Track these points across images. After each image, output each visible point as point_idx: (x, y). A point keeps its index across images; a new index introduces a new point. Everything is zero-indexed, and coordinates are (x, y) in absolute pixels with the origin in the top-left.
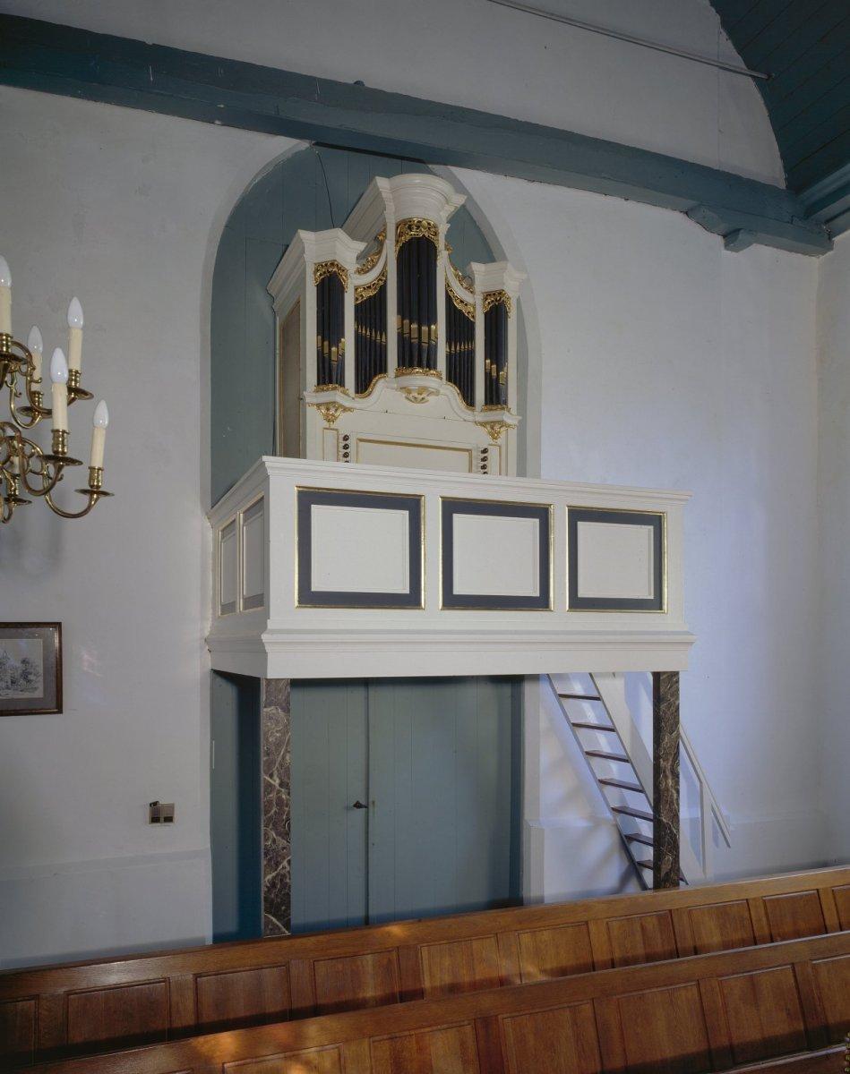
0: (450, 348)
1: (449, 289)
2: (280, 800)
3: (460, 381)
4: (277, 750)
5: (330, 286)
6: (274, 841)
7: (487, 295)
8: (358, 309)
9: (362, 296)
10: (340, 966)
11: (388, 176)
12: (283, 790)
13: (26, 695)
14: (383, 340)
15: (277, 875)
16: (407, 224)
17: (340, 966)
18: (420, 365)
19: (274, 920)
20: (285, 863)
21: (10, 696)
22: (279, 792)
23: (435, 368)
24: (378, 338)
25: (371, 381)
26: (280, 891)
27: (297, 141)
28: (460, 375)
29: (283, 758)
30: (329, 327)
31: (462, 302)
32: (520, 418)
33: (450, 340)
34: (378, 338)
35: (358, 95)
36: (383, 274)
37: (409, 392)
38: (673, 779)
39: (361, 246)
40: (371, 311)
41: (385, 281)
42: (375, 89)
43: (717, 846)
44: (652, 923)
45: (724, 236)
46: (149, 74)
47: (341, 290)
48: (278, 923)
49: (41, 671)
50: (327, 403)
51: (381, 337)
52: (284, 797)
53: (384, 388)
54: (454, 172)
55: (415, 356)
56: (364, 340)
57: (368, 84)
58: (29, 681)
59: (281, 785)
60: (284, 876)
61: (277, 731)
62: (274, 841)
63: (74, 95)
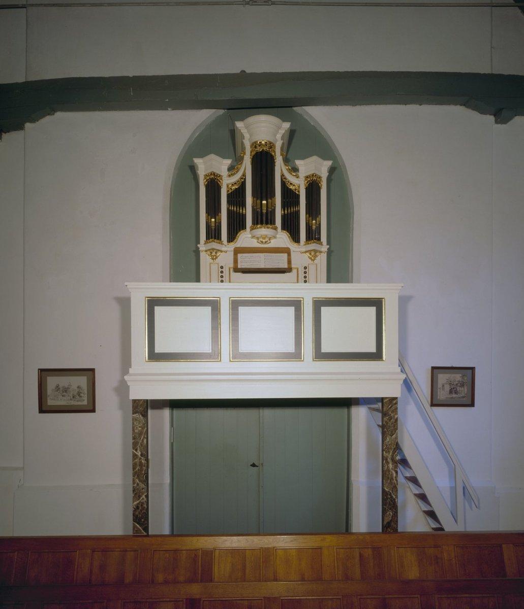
0: (284, 211)
1: (283, 177)
2: (141, 463)
3: (291, 229)
4: (139, 437)
5: (213, 185)
6: (138, 484)
7: (307, 177)
8: (229, 196)
9: (231, 189)
10: (167, 555)
11: (242, 119)
12: (143, 458)
13: (80, 403)
14: (244, 211)
15: (140, 502)
16: (254, 145)
17: (167, 555)
18: (262, 223)
19: (138, 526)
20: (144, 496)
21: (72, 404)
22: (140, 459)
23: (274, 224)
24: (241, 211)
25: (237, 234)
26: (141, 511)
27: (214, 110)
28: (291, 226)
29: (143, 441)
30: (213, 208)
31: (291, 184)
32: (328, 246)
33: (284, 206)
34: (241, 211)
35: (244, 78)
36: (244, 175)
37: (258, 238)
38: (392, 464)
39: (228, 162)
40: (237, 197)
41: (245, 179)
42: (145, 76)
43: (472, 509)
44: (368, 553)
45: (495, 115)
46: (130, 91)
47: (219, 188)
48: (140, 528)
49: (86, 392)
50: (209, 250)
51: (243, 210)
52: (143, 461)
53: (245, 238)
54: (221, 110)
55: (263, 218)
56: (233, 213)
57: (248, 71)
58: (81, 397)
59: (142, 455)
60: (143, 503)
61: (139, 427)
62: (138, 484)
63: (100, 110)
